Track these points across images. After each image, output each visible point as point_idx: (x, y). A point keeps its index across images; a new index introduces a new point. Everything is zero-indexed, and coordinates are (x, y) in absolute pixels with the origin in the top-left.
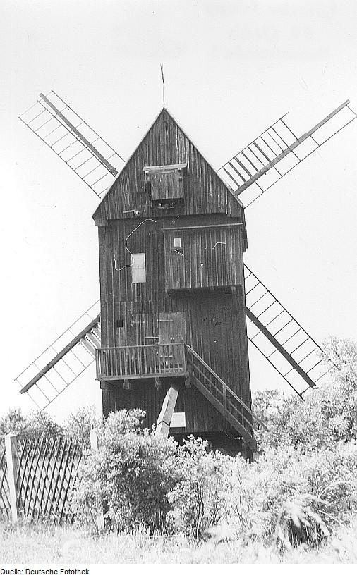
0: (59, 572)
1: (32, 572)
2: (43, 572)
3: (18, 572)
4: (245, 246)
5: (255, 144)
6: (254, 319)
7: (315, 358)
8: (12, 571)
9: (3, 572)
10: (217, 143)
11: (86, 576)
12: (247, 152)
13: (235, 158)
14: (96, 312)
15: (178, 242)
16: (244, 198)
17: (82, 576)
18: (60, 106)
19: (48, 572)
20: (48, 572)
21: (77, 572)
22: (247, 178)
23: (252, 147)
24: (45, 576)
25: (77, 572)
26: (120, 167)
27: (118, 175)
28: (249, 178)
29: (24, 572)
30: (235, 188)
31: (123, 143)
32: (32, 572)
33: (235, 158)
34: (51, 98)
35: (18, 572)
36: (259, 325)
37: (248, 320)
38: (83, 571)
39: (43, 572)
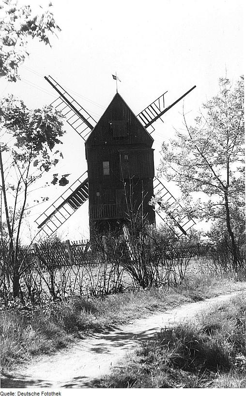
0: (40, 394)
1: (22, 394)
2: (30, 394)
3: (13, 394)
7: (68, 116)
8: (8, 393)
9: (2, 394)
12: (144, 112)
13: (150, 105)
14: (86, 176)
15: (126, 157)
16: (149, 130)
18: (70, 100)
19: (33, 394)
20: (33, 394)
22: (147, 123)
23: (150, 107)
26: (94, 125)
29: (16, 394)
30: (144, 125)
31: (96, 111)
32: (22, 394)
34: (40, 221)
35: (13, 394)
38: (57, 393)
39: (30, 394)
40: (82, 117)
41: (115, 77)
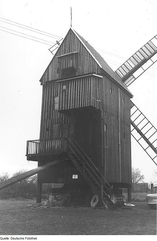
0: (25, 239)
1: (13, 239)
2: (18, 239)
3: (8, 239)
4: (131, 96)
5: (125, 65)
6: (136, 127)
8: (5, 238)
9: (1, 238)
10: (113, 51)
11: (36, 240)
17: (34, 240)
19: (20, 239)
20: (20, 239)
21: (32, 238)
24: (14, 240)
25: (32, 238)
27: (60, 45)
28: (123, 76)
29: (10, 239)
31: (42, 59)
32: (13, 239)
33: (141, 49)
35: (8, 239)
36: (139, 131)
37: (132, 128)
38: (35, 238)
39: (18, 239)
40: (147, 140)
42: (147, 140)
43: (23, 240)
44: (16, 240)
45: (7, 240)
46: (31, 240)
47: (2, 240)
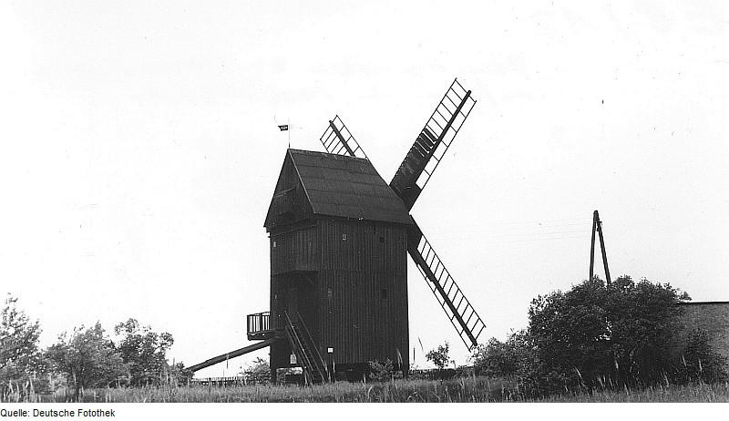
0: (76, 413)
1: (42, 413)
2: (56, 414)
3: (24, 413)
8: (16, 412)
9: (4, 413)
11: (110, 418)
17: (105, 418)
20: (62, 414)
24: (45, 418)
25: (99, 412)
38: (108, 412)
39: (56, 414)
40: (469, 333)
41: (284, 128)
42: (469, 333)
43: (70, 418)
44: (50, 418)
45: (22, 418)
46: (96, 418)
47: (7, 418)
